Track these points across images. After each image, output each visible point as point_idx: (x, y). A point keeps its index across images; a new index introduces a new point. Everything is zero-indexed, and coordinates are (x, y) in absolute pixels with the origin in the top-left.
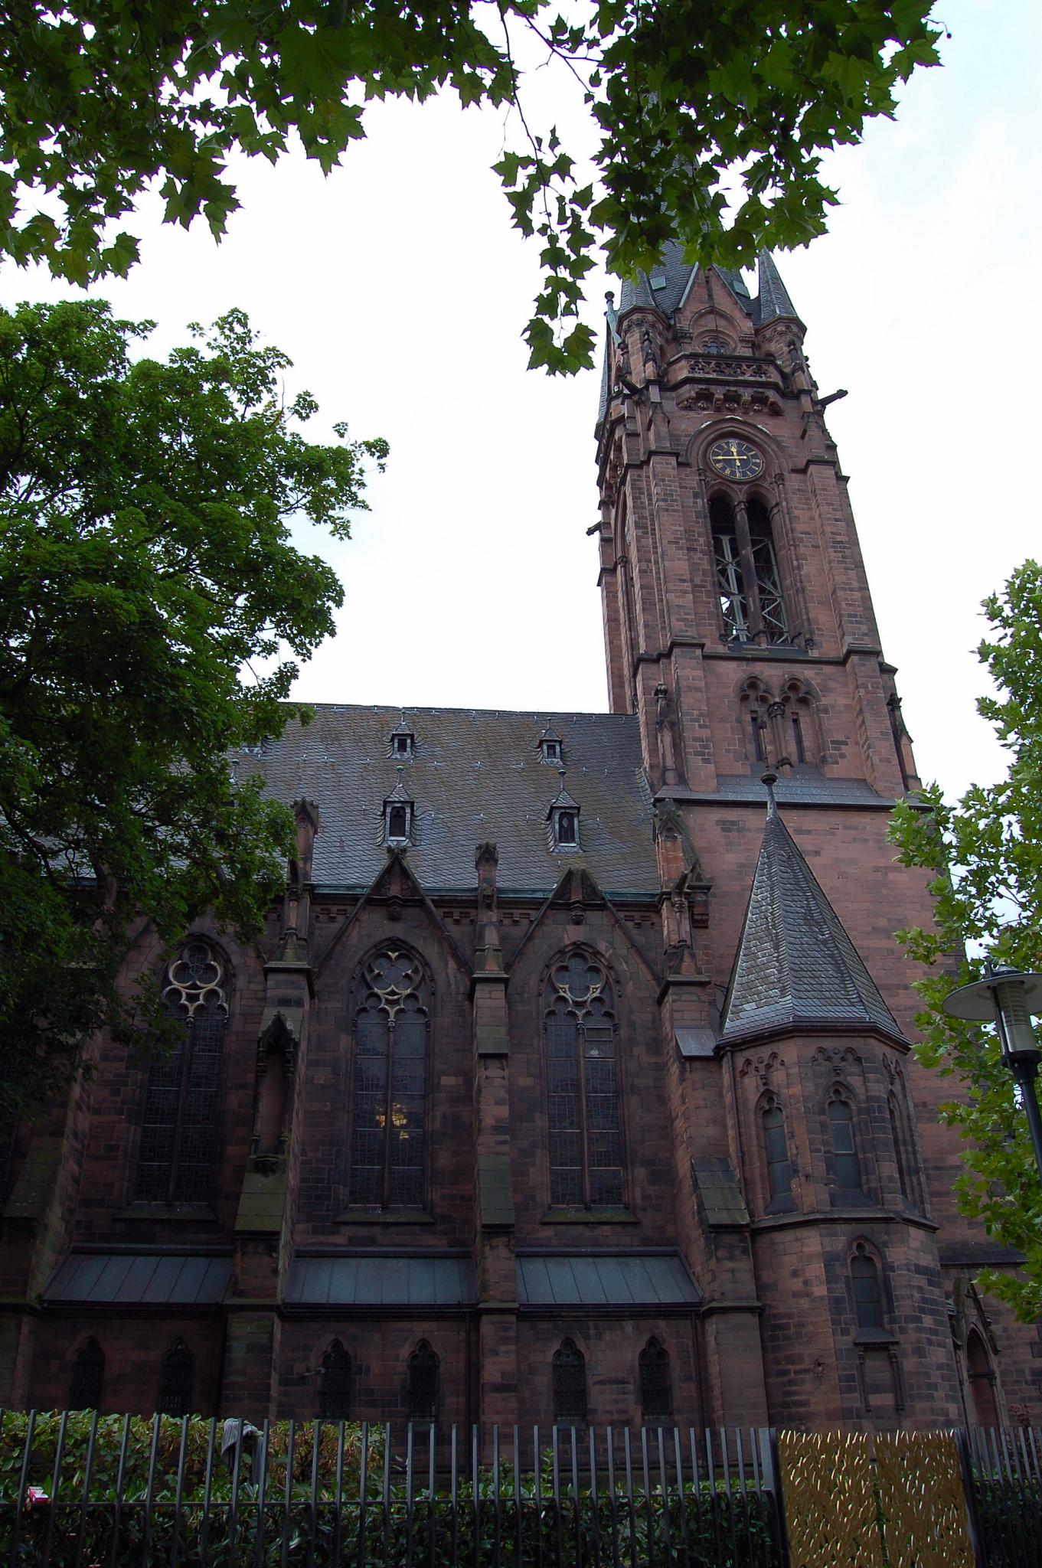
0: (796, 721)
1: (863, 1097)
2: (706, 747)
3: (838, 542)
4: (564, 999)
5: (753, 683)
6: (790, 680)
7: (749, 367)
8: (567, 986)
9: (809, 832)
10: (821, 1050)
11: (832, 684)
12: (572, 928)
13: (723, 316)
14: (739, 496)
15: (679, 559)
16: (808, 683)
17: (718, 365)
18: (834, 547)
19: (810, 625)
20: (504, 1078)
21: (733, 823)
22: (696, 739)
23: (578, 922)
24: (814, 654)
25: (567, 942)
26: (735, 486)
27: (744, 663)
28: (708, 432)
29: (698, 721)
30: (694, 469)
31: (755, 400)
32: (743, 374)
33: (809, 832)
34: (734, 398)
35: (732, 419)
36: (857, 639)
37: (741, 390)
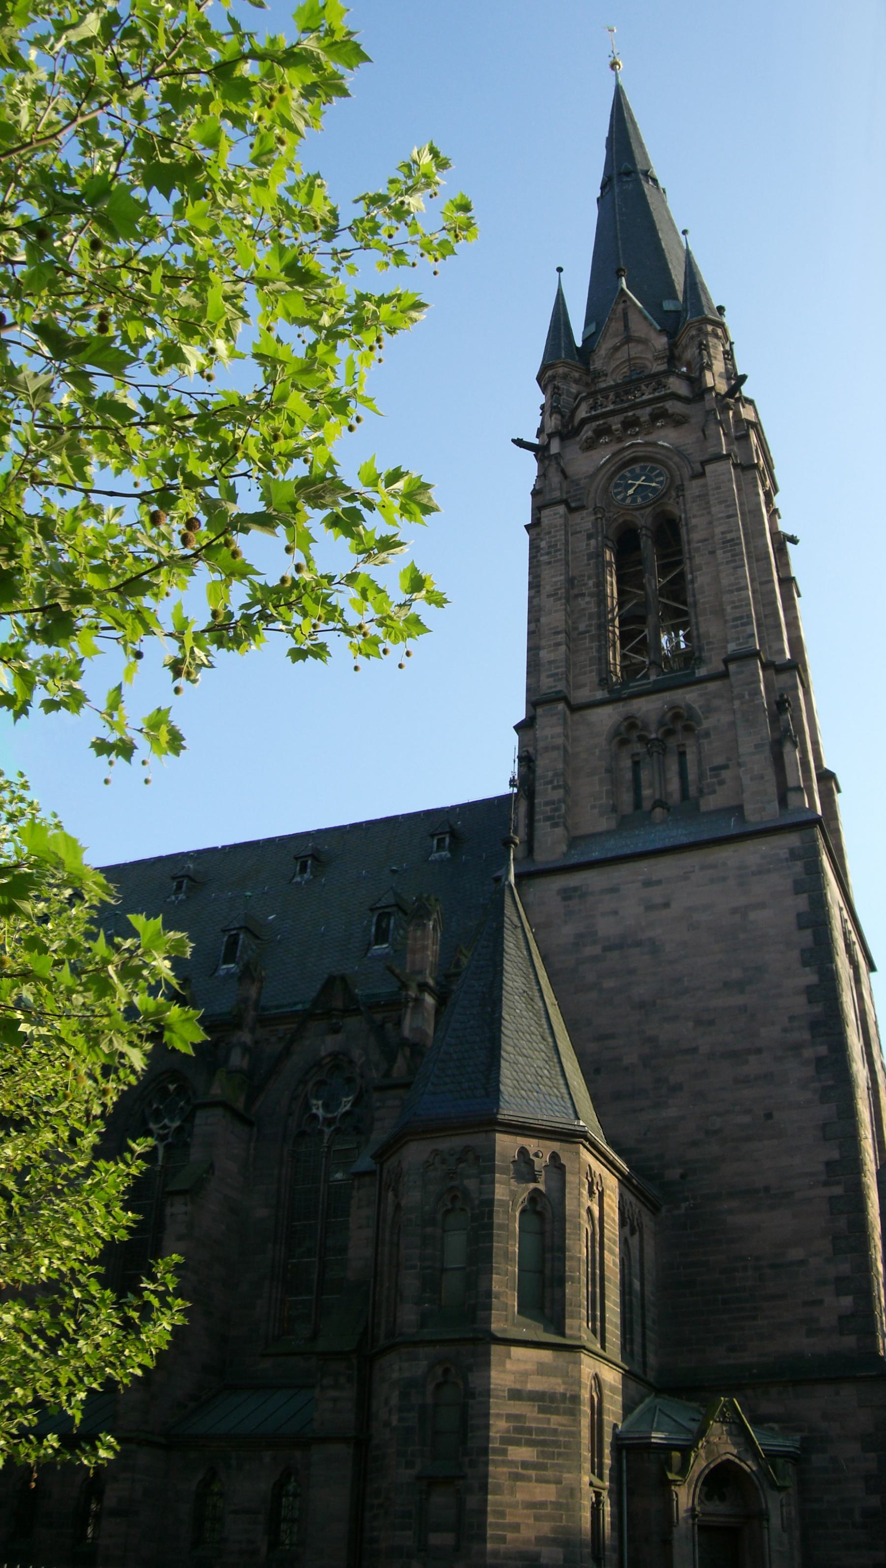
0: (682, 754)
1: (477, 1202)
2: (557, 809)
3: (729, 541)
4: (315, 1116)
5: (632, 722)
6: (671, 709)
7: (647, 386)
8: (320, 1102)
9: (659, 882)
10: (436, 1152)
11: (716, 702)
12: (329, 1039)
13: (639, 341)
14: (643, 520)
15: (556, 611)
16: (689, 708)
17: (617, 395)
18: (723, 548)
19: (699, 641)
20: (186, 1213)
21: (575, 889)
22: (547, 804)
23: (336, 1030)
24: (702, 672)
25: (323, 1053)
26: (637, 513)
27: (621, 704)
28: (608, 466)
29: (551, 782)
30: (591, 509)
31: (654, 417)
32: (643, 394)
33: (659, 882)
34: (628, 424)
35: (632, 445)
36: (740, 644)
37: (638, 412)
